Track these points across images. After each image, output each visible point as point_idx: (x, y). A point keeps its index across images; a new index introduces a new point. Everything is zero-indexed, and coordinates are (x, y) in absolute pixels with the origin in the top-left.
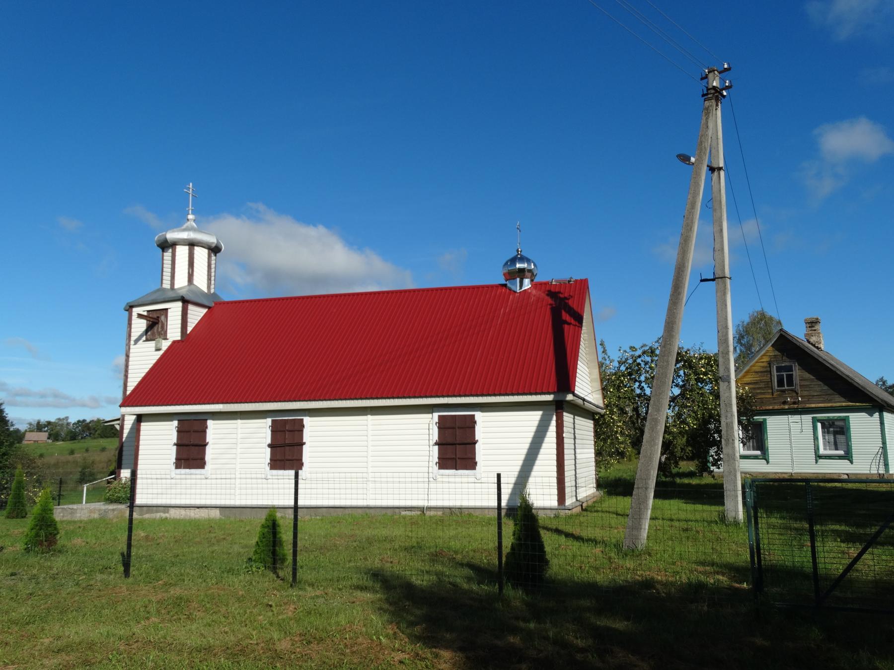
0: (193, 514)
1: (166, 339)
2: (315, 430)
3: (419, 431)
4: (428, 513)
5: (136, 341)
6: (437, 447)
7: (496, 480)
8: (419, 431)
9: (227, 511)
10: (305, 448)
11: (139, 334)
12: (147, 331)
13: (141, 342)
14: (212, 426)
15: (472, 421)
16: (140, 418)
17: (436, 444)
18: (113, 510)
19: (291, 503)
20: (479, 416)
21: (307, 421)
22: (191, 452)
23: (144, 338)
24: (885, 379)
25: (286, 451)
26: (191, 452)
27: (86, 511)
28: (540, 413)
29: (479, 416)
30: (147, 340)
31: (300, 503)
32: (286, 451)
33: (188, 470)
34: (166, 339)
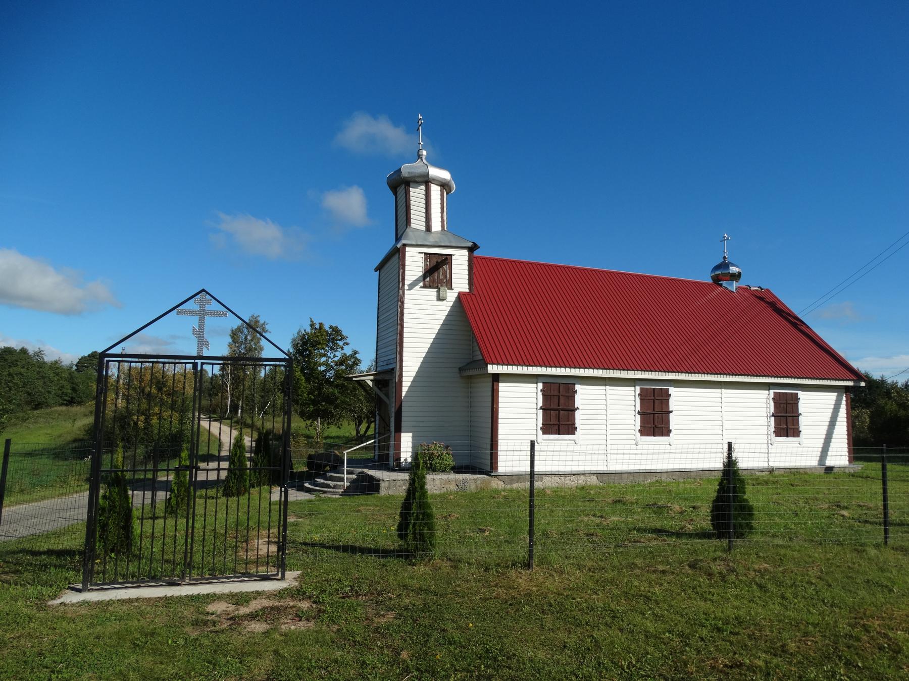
0: (568, 482)
1: (451, 289)
2: (681, 400)
3: (757, 405)
4: (776, 473)
5: (412, 286)
6: (773, 419)
7: (529, 448)
8: (757, 405)
9: (606, 478)
10: (672, 416)
11: (415, 278)
12: (425, 276)
13: (417, 287)
14: (504, 388)
15: (796, 399)
16: (202, 364)
17: (541, 408)
18: (475, 480)
19: (528, 469)
20: (801, 395)
21: (672, 390)
22: (559, 416)
23: (422, 284)
24: (334, 325)
25: (655, 419)
26: (559, 416)
27: (438, 483)
28: (836, 394)
29: (801, 395)
30: (425, 287)
31: (536, 469)
32: (655, 419)
33: (557, 436)
34: (451, 289)
